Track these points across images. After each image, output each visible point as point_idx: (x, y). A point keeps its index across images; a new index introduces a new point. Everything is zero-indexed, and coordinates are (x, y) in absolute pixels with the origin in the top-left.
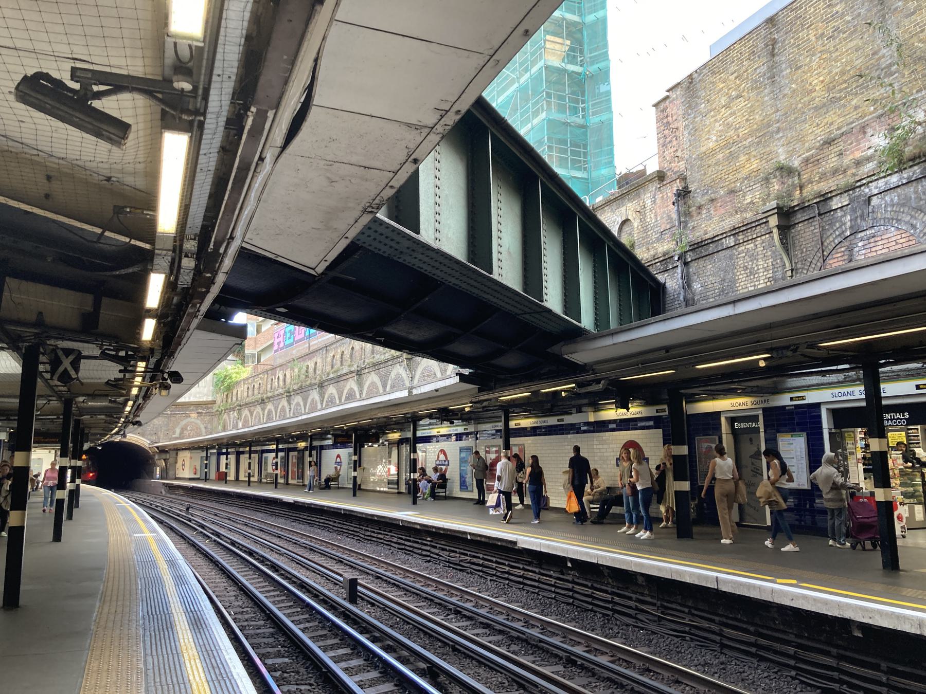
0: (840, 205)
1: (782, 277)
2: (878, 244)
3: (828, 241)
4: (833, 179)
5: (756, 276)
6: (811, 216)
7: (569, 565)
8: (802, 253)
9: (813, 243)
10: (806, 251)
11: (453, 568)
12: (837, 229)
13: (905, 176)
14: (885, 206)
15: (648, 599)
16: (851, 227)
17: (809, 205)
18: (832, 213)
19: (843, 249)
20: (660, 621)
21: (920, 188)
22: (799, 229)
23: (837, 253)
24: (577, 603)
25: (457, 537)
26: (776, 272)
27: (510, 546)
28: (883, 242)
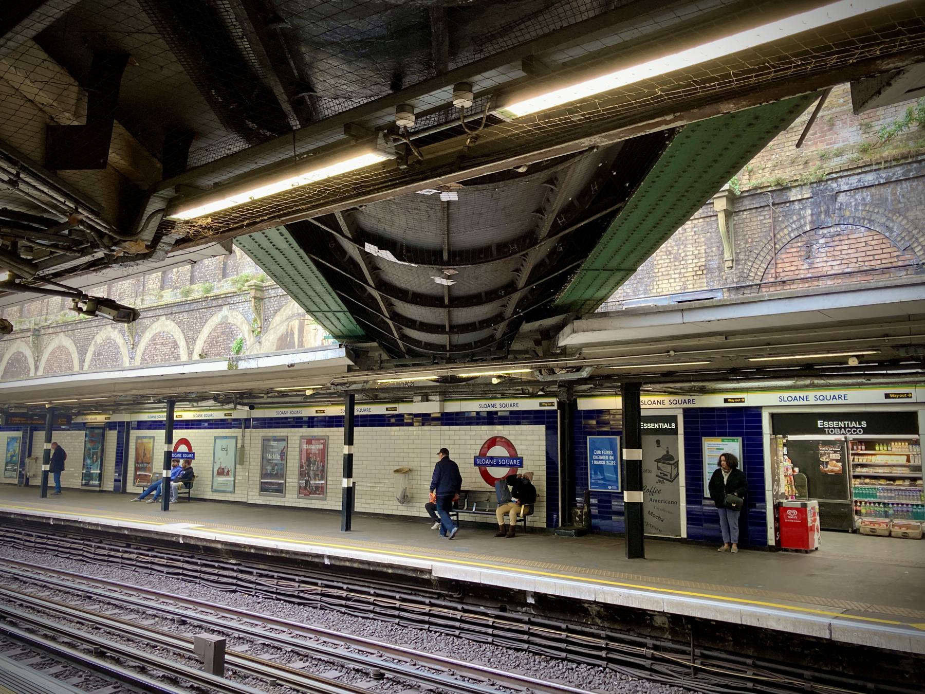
0: (800, 197)
1: (718, 267)
2: (843, 243)
3: (782, 234)
4: (792, 168)
5: (683, 262)
6: (763, 204)
7: (531, 600)
8: (746, 243)
9: (762, 234)
10: (752, 242)
11: (285, 601)
12: (794, 222)
13: (884, 175)
14: (855, 205)
15: (669, 644)
16: (812, 222)
17: (761, 193)
18: (788, 205)
19: (799, 244)
20: (695, 674)
21: (899, 190)
22: (744, 216)
23: (792, 248)
24: (534, 648)
25: (296, 560)
26: (710, 260)
27: (317, 560)
28: (850, 242)
